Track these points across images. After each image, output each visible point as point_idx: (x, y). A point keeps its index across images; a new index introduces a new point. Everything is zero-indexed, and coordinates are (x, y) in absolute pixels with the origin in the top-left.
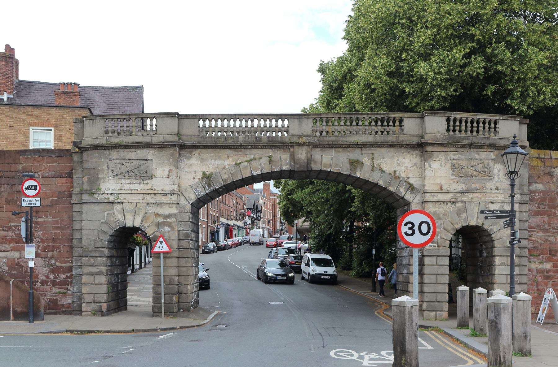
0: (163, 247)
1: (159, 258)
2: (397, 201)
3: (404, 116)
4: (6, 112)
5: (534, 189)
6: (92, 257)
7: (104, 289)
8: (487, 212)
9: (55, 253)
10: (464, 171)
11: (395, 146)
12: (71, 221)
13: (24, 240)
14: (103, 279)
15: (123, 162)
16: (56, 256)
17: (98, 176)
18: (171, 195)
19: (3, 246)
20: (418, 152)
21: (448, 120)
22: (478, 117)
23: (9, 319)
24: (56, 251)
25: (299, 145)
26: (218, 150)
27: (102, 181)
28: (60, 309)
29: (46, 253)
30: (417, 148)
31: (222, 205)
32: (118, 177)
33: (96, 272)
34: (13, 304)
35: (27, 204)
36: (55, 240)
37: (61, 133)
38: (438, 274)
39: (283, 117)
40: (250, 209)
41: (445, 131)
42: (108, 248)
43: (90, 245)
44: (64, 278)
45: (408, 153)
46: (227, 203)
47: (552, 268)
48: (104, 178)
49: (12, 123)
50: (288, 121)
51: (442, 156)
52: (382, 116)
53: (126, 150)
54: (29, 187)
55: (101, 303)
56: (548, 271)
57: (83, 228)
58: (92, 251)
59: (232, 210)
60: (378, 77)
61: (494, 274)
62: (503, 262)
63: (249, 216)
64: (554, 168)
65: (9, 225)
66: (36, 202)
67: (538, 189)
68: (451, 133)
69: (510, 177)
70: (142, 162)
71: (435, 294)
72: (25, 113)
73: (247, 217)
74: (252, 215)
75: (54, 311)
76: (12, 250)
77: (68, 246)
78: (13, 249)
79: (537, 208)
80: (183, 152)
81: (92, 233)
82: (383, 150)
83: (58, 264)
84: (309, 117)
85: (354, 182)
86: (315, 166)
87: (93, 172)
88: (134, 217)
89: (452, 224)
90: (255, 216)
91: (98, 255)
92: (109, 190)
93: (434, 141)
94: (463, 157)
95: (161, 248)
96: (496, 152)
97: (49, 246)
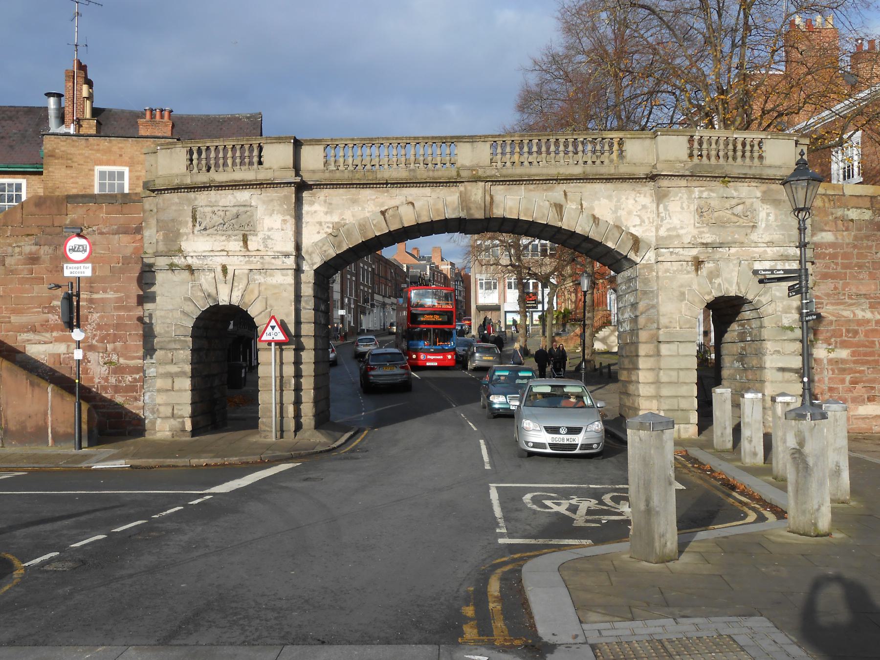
0: (276, 334)
2: (617, 262)
5: (819, 241)
6: (170, 349)
9: (118, 344)
18: (285, 258)
21: (691, 140)
22: (735, 136)
24: (119, 342)
27: (185, 237)
31: (376, 278)
32: (208, 232)
34: (52, 421)
35: (71, 273)
36: (117, 326)
37: (138, 174)
38: (681, 369)
41: (687, 156)
43: (167, 332)
44: (131, 382)
47: (850, 358)
48: (187, 234)
51: (683, 194)
54: (75, 247)
55: (184, 417)
56: (843, 361)
58: (170, 342)
59: (390, 284)
60: (505, 640)
61: (765, 368)
62: (777, 349)
64: (848, 210)
65: (52, 305)
66: (85, 270)
67: (825, 240)
68: (696, 160)
69: (797, 217)
70: (242, 209)
76: (56, 341)
77: (137, 334)
78: (58, 340)
79: (825, 268)
81: (171, 314)
83: (122, 361)
84: (486, 139)
85: (554, 235)
92: (195, 252)
93: (671, 171)
95: (273, 336)
96: (764, 187)
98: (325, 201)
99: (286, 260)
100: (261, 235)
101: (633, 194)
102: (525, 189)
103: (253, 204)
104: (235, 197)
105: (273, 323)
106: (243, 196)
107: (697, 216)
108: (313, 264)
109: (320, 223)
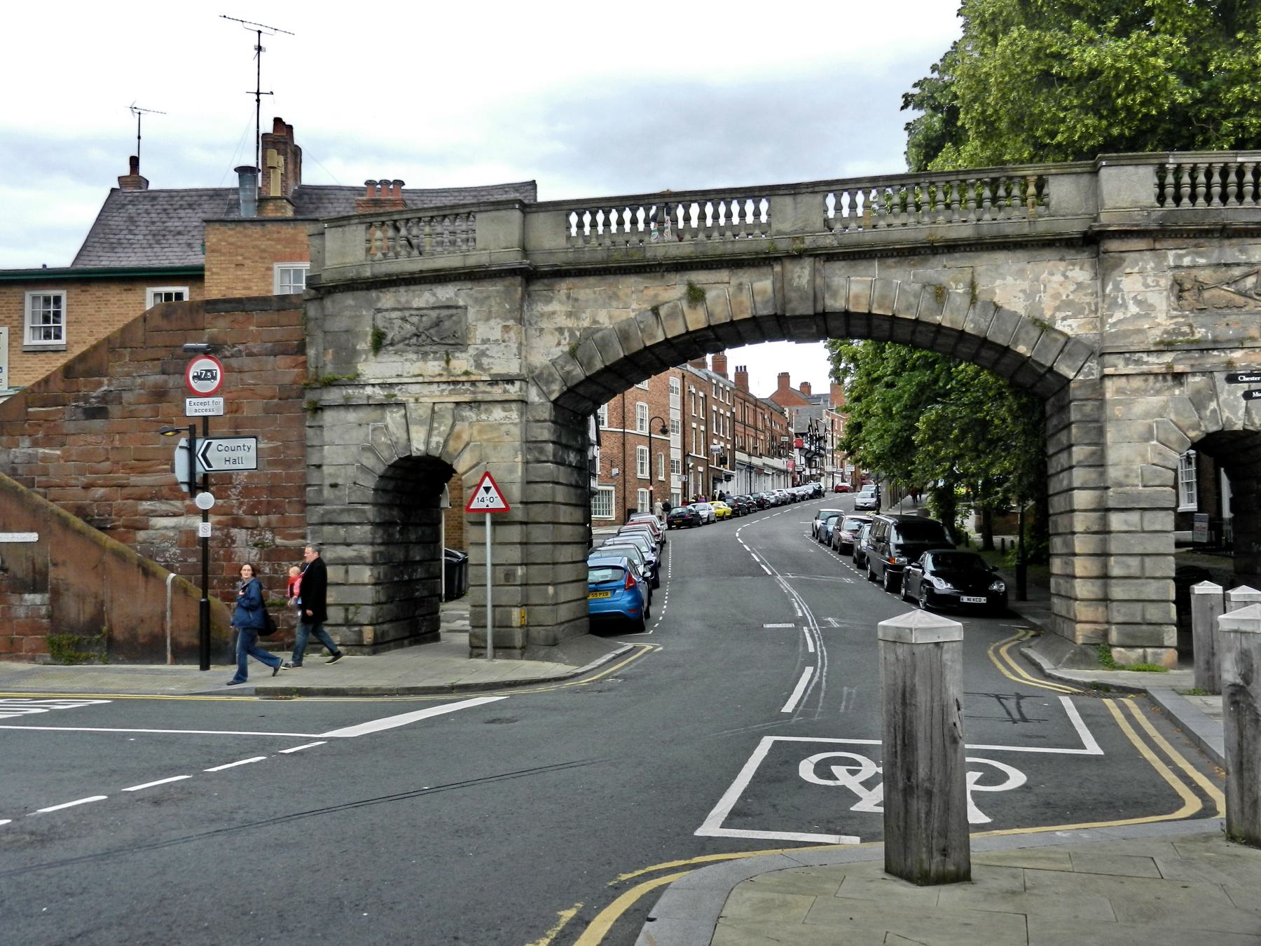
1: (483, 524)
3: (1048, 172)
4: (230, 236)
7: (368, 594)
8: (1245, 379)
10: (1206, 294)
11: (1026, 246)
12: (304, 446)
13: (185, 488)
14: (366, 574)
15: (407, 314)
16: (274, 524)
17: (354, 346)
19: (173, 505)
20: (1085, 255)
21: (1161, 171)
22: (1240, 159)
23: (163, 660)
25: (799, 255)
26: (611, 279)
27: (364, 357)
28: (282, 639)
29: (254, 518)
30: (1083, 246)
33: (351, 558)
36: (272, 490)
39: (757, 194)
40: (803, 434)
42: (374, 504)
45: (1061, 260)
46: (751, 422)
49: (240, 258)
50: (769, 201)
52: (993, 175)
53: (412, 288)
57: (326, 461)
58: (342, 511)
59: (762, 437)
63: (801, 449)
70: (445, 312)
71: (1140, 604)
72: (265, 236)
73: (797, 451)
74: (807, 446)
75: (271, 643)
80: (536, 287)
82: (1000, 257)
83: (279, 541)
86: (833, 302)
87: (344, 337)
88: (429, 435)
89: (1180, 428)
90: (813, 448)
91: (354, 520)
94: (1202, 261)
95: (487, 502)
97: (260, 502)
98: (568, 297)
99: (509, 387)
100: (471, 351)
101: (1062, 266)
102: (879, 265)
103: (461, 303)
104: (434, 295)
105: (487, 483)
106: (445, 293)
107: (1172, 299)
108: (551, 393)
109: (560, 330)
